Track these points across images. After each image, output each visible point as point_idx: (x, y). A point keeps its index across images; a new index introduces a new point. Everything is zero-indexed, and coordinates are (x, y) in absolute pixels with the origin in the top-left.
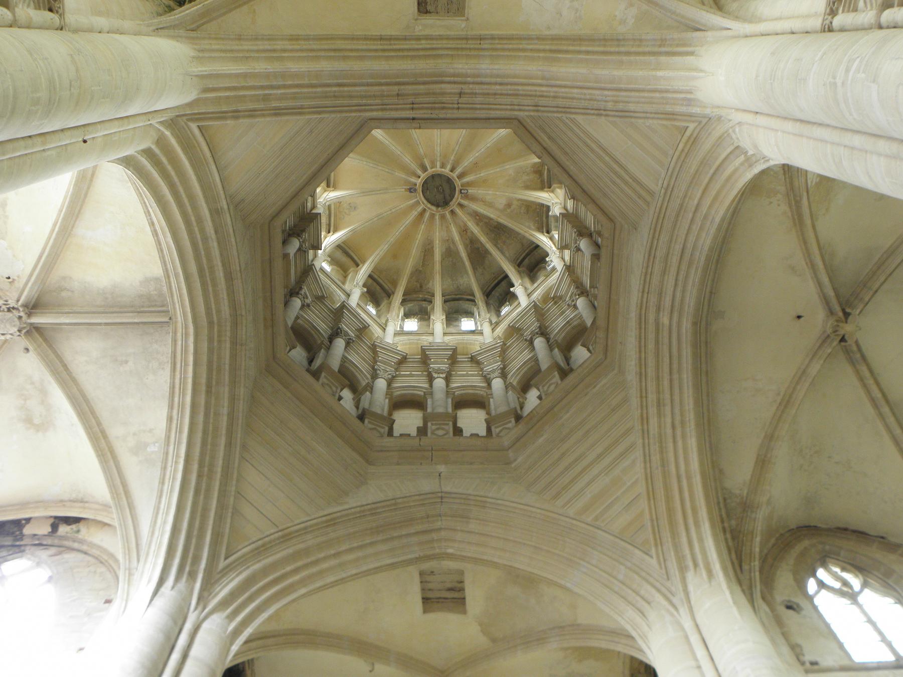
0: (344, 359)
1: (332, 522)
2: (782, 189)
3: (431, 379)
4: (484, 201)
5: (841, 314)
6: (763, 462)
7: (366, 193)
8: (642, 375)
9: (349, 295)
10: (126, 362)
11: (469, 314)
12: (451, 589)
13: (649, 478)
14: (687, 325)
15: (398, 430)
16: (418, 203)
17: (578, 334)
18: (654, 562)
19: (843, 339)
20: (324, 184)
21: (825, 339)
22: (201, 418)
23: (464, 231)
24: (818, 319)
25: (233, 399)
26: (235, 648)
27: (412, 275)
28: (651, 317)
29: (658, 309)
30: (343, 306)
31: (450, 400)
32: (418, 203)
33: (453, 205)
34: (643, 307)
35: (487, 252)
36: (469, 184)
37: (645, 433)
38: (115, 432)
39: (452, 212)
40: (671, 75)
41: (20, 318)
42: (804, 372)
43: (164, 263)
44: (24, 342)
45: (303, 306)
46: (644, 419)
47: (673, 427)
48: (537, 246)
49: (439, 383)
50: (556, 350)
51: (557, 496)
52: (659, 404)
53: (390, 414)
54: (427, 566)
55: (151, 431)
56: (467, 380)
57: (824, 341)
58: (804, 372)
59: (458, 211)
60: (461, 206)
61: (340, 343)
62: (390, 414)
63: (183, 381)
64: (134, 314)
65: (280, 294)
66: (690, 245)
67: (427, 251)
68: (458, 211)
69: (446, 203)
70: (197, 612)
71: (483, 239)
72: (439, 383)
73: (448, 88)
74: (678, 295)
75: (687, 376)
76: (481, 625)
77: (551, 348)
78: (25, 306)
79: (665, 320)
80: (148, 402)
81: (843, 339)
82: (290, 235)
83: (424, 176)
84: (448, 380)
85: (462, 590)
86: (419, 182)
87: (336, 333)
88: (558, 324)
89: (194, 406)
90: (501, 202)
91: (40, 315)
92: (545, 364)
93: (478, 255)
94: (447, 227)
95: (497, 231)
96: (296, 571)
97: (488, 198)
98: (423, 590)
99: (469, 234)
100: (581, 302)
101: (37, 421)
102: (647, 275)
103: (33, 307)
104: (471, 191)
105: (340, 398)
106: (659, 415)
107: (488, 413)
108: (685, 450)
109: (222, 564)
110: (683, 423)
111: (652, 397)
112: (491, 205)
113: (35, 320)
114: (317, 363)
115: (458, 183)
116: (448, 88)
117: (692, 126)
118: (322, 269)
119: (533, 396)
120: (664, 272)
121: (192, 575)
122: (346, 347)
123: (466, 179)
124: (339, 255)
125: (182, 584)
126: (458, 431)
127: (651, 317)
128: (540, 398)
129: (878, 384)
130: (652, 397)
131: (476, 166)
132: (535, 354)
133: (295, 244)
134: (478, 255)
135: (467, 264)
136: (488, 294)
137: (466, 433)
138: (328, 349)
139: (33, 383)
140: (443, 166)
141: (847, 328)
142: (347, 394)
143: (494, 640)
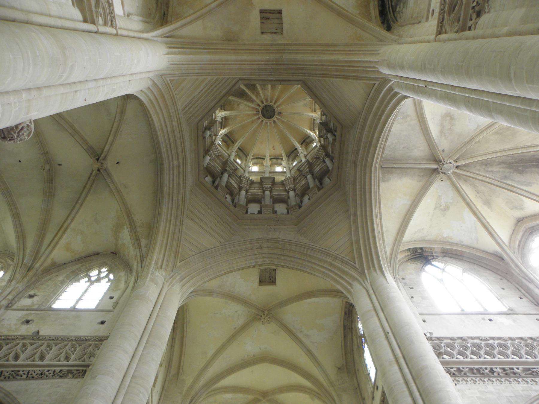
0: (227, 182)
3: (264, 192)
5: (102, 171)
7: (299, 114)
8: (182, 138)
9: (230, 156)
10: (403, 148)
11: (280, 164)
12: (268, 18)
14: (166, 165)
15: (249, 211)
16: (277, 107)
17: (326, 172)
18: (168, 79)
19: (98, 160)
20: (219, 109)
24: (109, 164)
25: (361, 134)
28: (181, 160)
29: (179, 167)
30: (227, 160)
31: (272, 200)
33: (262, 106)
36: (256, 115)
38: (415, 122)
41: (441, 169)
45: (210, 160)
46: (179, 123)
47: (166, 126)
48: (309, 136)
49: (267, 193)
50: (316, 180)
52: (173, 131)
53: (247, 205)
54: (279, 39)
55: (399, 123)
56: (279, 192)
60: (259, 105)
61: (226, 176)
62: (247, 205)
64: (396, 166)
65: (202, 153)
68: (260, 104)
71: (249, 93)
72: (267, 193)
73: (266, 250)
74: (171, 176)
76: (252, 4)
77: (314, 179)
78: (438, 172)
79: (175, 162)
80: (400, 132)
81: (98, 160)
82: (205, 129)
83: (274, 118)
84: (271, 192)
85: (262, 18)
86: (276, 116)
87: (224, 171)
88: (318, 169)
90: (242, 107)
92: (311, 185)
94: (265, 95)
97: (247, 109)
99: (255, 92)
100: (327, 160)
101: (449, 118)
105: (226, 198)
107: (288, 206)
111: (177, 132)
112: (246, 105)
113: (434, 166)
114: (216, 183)
115: (260, 115)
117: (178, 264)
118: (219, 144)
119: (306, 199)
120: (178, 185)
122: (228, 177)
124: (226, 138)
126: (275, 212)
128: (309, 199)
129: (66, 19)
130: (177, 132)
131: (253, 122)
132: (308, 182)
133: (208, 133)
136: (288, 156)
137: (278, 213)
138: (221, 178)
139: (445, 136)
141: (97, 166)
142: (228, 197)
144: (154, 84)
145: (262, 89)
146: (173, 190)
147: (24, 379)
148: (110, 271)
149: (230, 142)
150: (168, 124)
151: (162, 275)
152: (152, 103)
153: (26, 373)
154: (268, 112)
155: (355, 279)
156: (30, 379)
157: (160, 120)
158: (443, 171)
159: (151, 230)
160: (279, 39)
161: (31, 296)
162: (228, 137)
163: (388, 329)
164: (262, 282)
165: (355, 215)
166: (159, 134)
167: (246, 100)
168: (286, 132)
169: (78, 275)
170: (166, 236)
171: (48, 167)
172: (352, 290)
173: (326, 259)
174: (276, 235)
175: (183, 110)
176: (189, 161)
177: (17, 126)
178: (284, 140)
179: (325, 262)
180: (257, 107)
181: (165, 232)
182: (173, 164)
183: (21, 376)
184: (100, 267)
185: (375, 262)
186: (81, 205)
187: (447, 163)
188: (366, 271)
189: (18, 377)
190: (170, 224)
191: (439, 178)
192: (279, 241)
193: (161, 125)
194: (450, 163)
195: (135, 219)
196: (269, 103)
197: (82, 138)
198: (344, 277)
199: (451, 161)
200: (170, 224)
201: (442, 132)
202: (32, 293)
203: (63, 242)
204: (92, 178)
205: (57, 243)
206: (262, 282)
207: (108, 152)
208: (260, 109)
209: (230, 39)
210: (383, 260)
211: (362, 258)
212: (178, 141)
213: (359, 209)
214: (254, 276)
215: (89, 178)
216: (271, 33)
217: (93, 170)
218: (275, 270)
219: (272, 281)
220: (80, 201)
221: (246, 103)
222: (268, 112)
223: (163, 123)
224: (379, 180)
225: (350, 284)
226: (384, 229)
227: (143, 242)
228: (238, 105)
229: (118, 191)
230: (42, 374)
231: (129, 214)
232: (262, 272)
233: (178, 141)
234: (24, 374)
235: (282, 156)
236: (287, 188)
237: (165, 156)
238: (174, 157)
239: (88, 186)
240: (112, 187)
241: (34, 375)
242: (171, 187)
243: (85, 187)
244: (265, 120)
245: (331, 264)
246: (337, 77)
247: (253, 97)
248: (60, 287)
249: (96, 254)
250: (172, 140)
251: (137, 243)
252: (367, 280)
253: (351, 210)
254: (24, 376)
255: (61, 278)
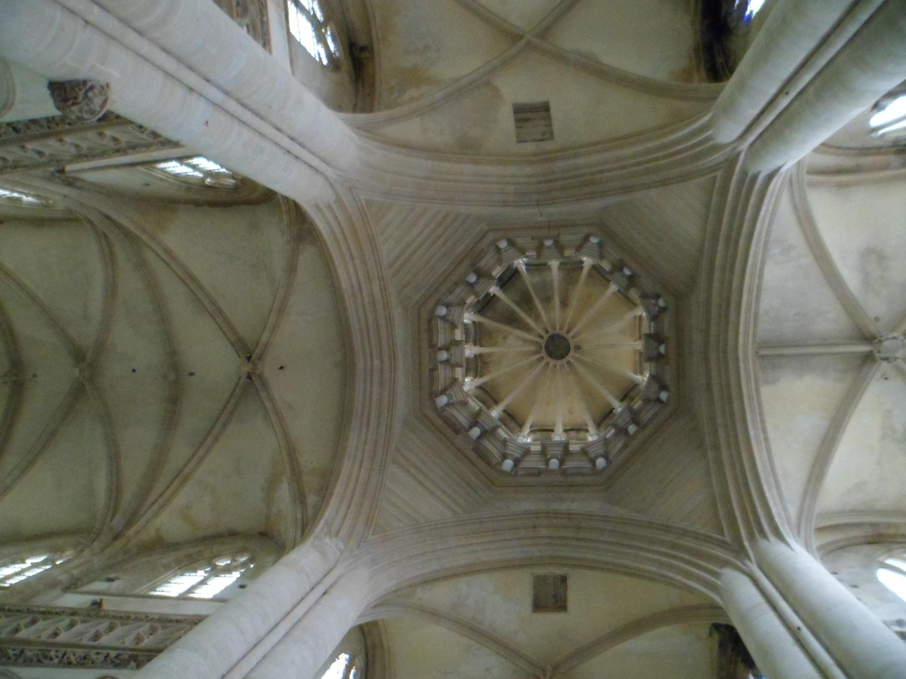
1: (628, 190)
2: (305, 478)
4: (525, 341)
5: (253, 378)
6: (292, 269)
8: (389, 319)
10: (795, 315)
12: (527, 120)
13: (374, 249)
14: (360, 365)
18: (362, 197)
19: (249, 359)
21: (260, 358)
22: (735, 283)
23: (537, 318)
24: (268, 370)
25: (709, 290)
26: (706, 118)
27: (577, 280)
28: (386, 362)
29: (382, 371)
32: (573, 337)
33: (546, 336)
34: (393, 369)
35: (518, 303)
36: (536, 353)
37: (381, 279)
38: (807, 260)
39: (547, 332)
40: (386, 583)
41: (879, 352)
42: (272, 332)
43: (758, 395)
44: (873, 328)
46: (383, 289)
51: (447, 216)
52: (373, 304)
54: (548, 146)
57: (262, 354)
58: (272, 332)
59: (543, 333)
60: (542, 337)
63: (748, 310)
66: (364, 429)
67: (564, 303)
68: (543, 333)
69: (553, 338)
70: (739, 149)
73: (543, 532)
75: (355, 328)
79: (376, 362)
80: (780, 282)
81: (249, 359)
83: (569, 358)
86: (572, 353)
89: (740, 294)
90: (511, 340)
91: (863, 350)
93: (525, 301)
95: (512, 320)
96: (657, 159)
98: (551, 126)
102: (393, 394)
103: (868, 359)
104: (533, 348)
106: (373, 296)
108: (350, 278)
109: (719, 174)
110: (354, 295)
111: (380, 306)
112: (519, 338)
113: (864, 348)
115: (543, 353)
116: (543, 532)
117: (370, 537)
120: (380, 401)
121: (744, 173)
123: (538, 356)
125: (752, 171)
127: (386, 362)
130: (380, 306)
131: (531, 366)
134: (525, 301)
135: (534, 296)
140: (555, 366)
141: (247, 368)
143: (488, 83)
144: (339, 201)
145: (546, 309)
146: (370, 411)
147: (54, 666)
148: (251, 560)
149: (491, 402)
150: (364, 287)
151: (336, 546)
152: (335, 235)
153: (60, 656)
154: (557, 347)
155: (725, 563)
156: (64, 667)
157: (350, 278)
158: (883, 355)
159: (327, 480)
160: (548, 146)
161: (111, 580)
162: (486, 392)
163: (796, 621)
164: (538, 606)
165: (716, 447)
166: (349, 302)
167: (519, 328)
168: (591, 379)
169: (195, 561)
170: (351, 485)
171: (172, 377)
172: (719, 583)
173: (663, 537)
174: (564, 507)
175: (391, 265)
176: (400, 365)
177: (85, 82)
178: (588, 395)
179: (662, 543)
180: (538, 340)
181: (349, 478)
182: (372, 365)
183: (51, 659)
184: (234, 555)
185: (764, 521)
186: (216, 439)
187: (888, 339)
188: (746, 544)
189: (46, 662)
190: (361, 466)
191: (879, 374)
192: (569, 515)
193: (352, 287)
194: (894, 338)
195: (302, 460)
196: (557, 331)
197: (228, 322)
198: (702, 563)
199: (895, 334)
200: (361, 466)
201: (866, 282)
202: (112, 576)
203: (180, 501)
204: (238, 391)
205: (168, 501)
206: (538, 606)
207: (267, 345)
208: (543, 342)
209: (467, 148)
210: (780, 517)
211: (738, 523)
212: (382, 322)
213: (721, 433)
214: (522, 586)
215: (232, 394)
216: (535, 141)
217: (240, 378)
218: (564, 579)
219: (560, 605)
220: (215, 431)
221: (518, 332)
222: (557, 347)
223: (354, 280)
224: (756, 381)
225: (716, 574)
226: (779, 472)
227: (312, 499)
228: (505, 338)
229: (278, 414)
230: (85, 658)
231: (292, 453)
232: (539, 582)
233: (382, 322)
234: (57, 657)
235: (586, 425)
236: (592, 455)
237: (358, 347)
238: (374, 352)
239: (230, 406)
240: (268, 405)
241: (73, 658)
242: (367, 404)
243: (225, 407)
244: (553, 362)
245: (674, 546)
246: (648, 186)
247: (530, 321)
248: (161, 574)
249: (233, 534)
250: (370, 318)
251: (300, 497)
252: (750, 560)
253: (708, 440)
254: (56, 661)
255: (165, 561)
